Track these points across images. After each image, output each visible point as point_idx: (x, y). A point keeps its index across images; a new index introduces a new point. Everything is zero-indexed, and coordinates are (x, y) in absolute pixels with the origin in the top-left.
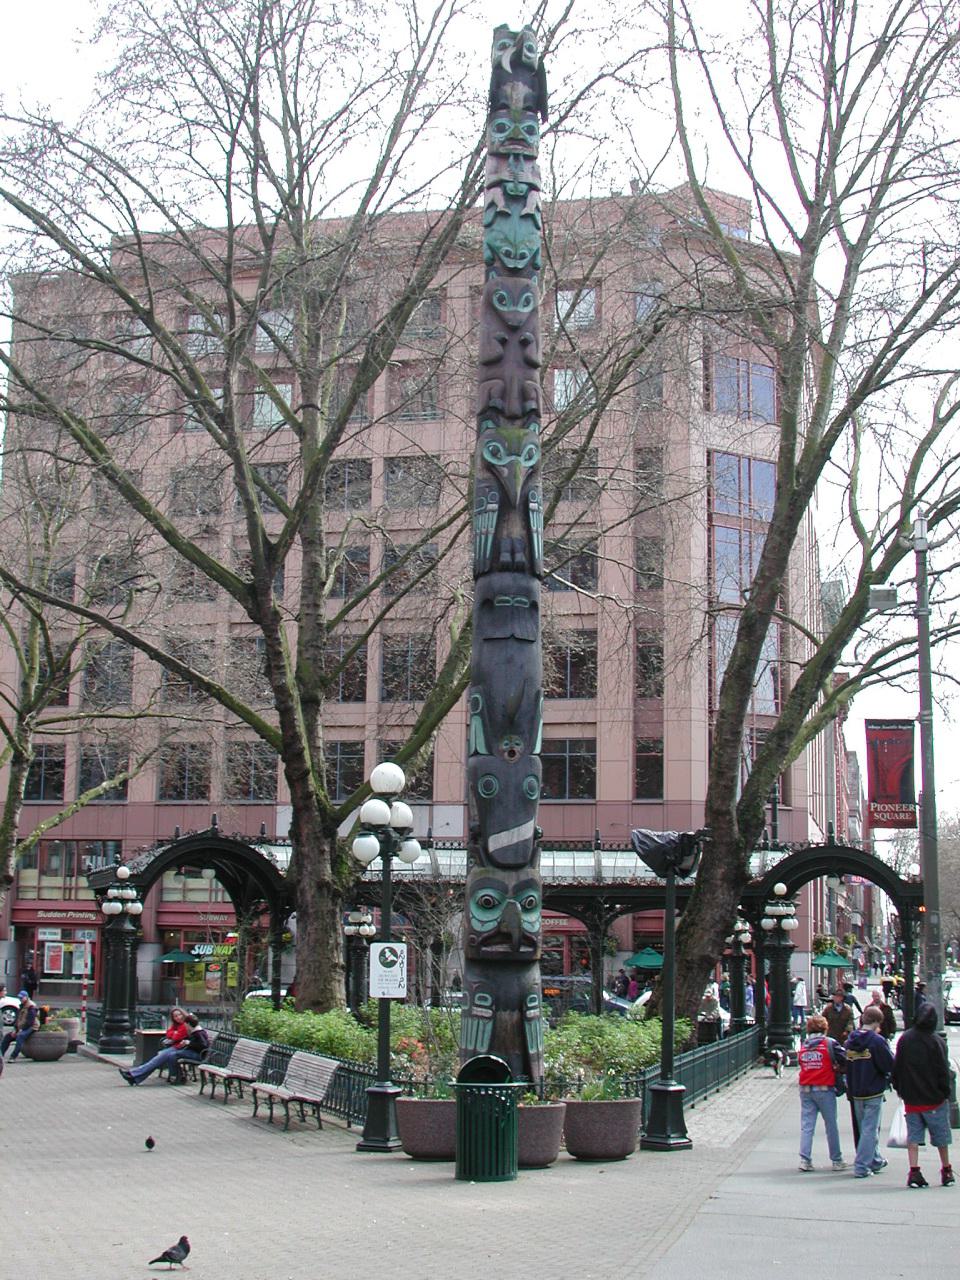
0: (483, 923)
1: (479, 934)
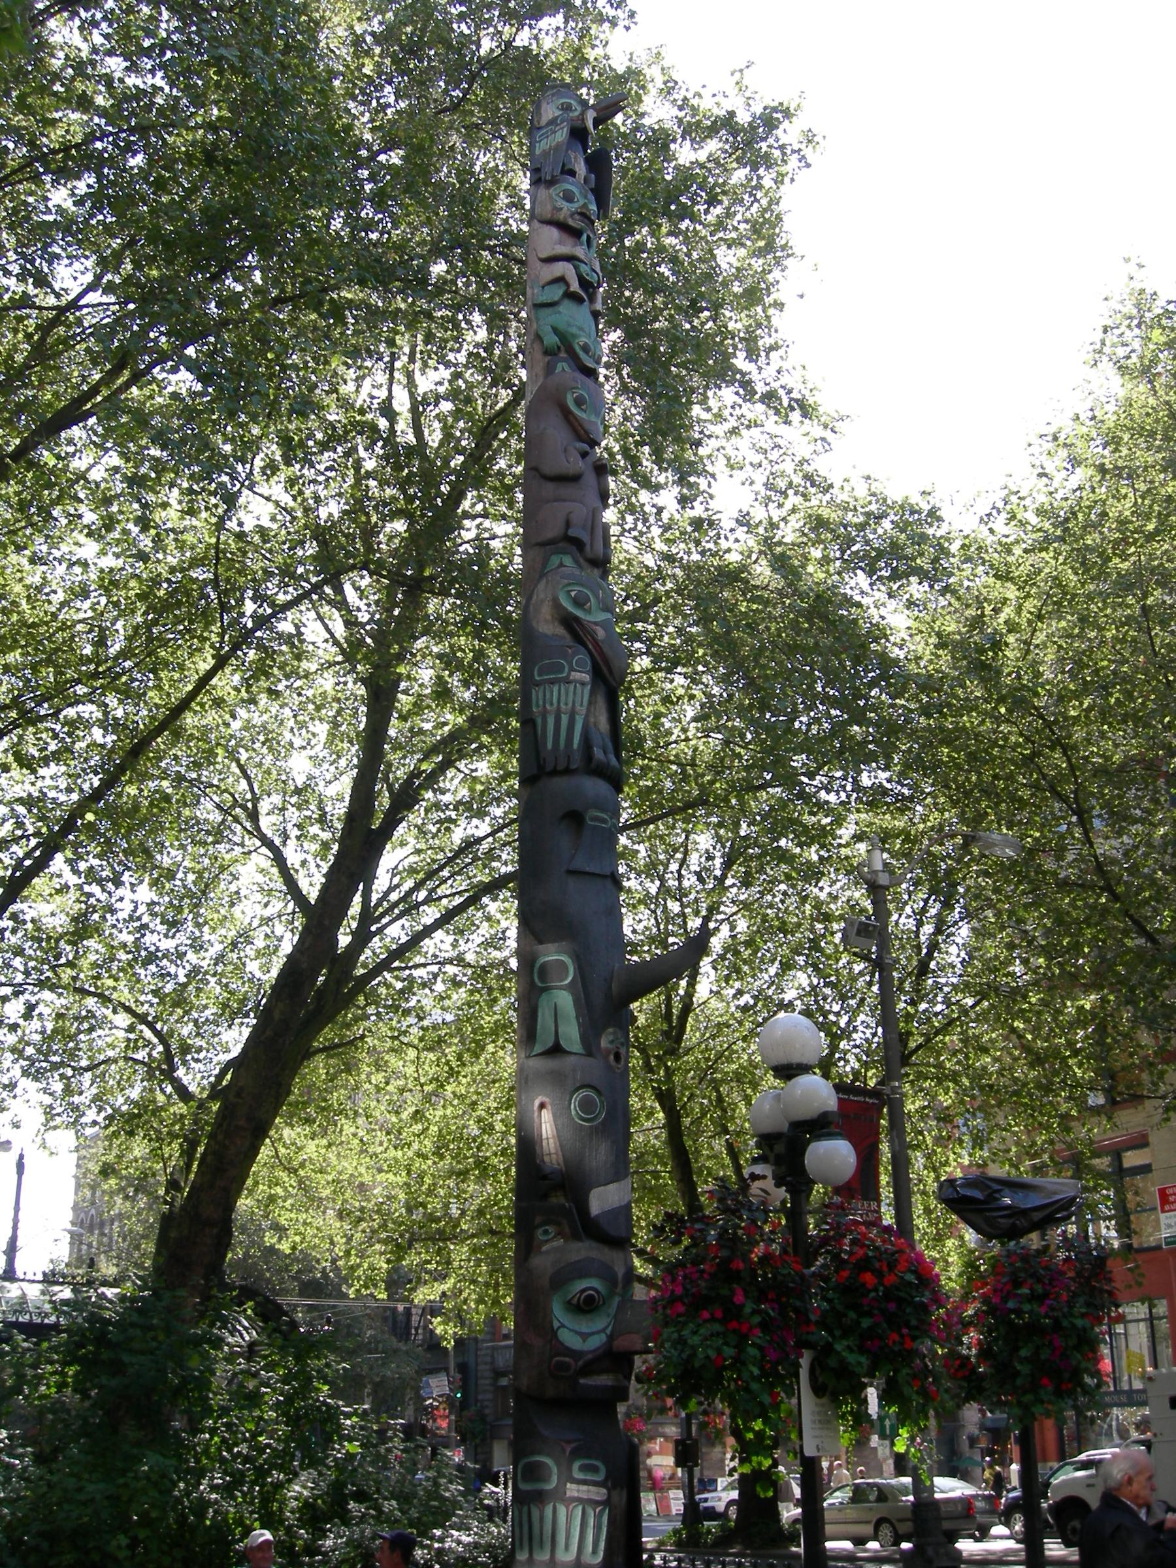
0: (585, 1336)
1: (575, 1354)
